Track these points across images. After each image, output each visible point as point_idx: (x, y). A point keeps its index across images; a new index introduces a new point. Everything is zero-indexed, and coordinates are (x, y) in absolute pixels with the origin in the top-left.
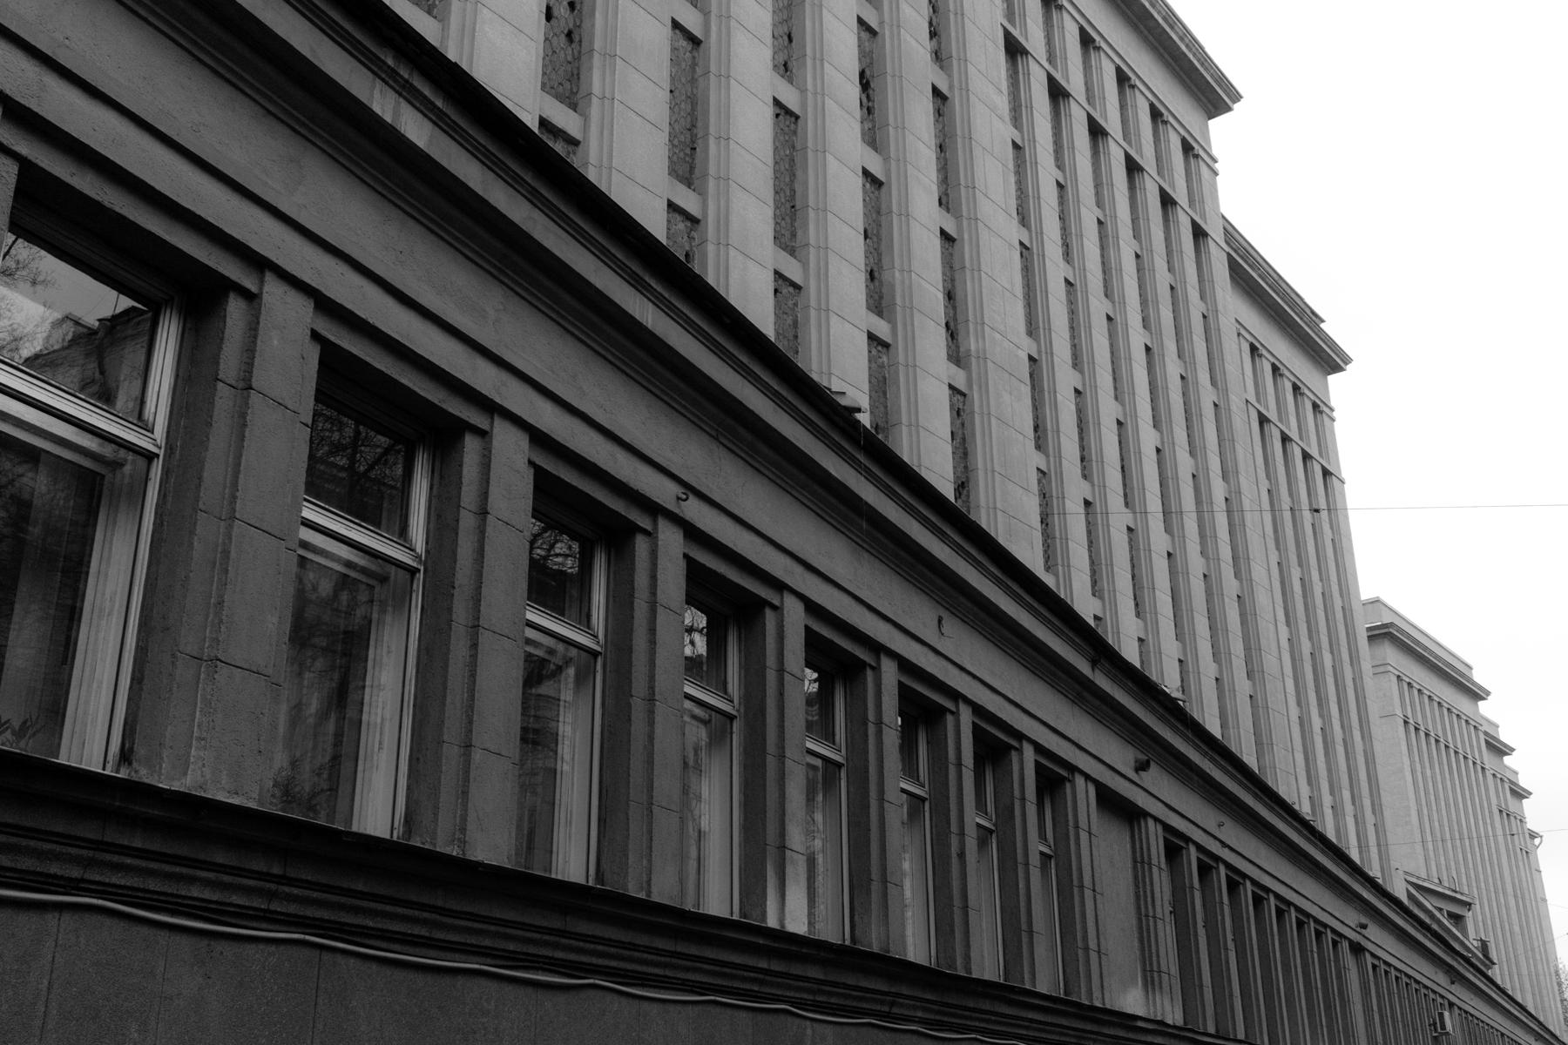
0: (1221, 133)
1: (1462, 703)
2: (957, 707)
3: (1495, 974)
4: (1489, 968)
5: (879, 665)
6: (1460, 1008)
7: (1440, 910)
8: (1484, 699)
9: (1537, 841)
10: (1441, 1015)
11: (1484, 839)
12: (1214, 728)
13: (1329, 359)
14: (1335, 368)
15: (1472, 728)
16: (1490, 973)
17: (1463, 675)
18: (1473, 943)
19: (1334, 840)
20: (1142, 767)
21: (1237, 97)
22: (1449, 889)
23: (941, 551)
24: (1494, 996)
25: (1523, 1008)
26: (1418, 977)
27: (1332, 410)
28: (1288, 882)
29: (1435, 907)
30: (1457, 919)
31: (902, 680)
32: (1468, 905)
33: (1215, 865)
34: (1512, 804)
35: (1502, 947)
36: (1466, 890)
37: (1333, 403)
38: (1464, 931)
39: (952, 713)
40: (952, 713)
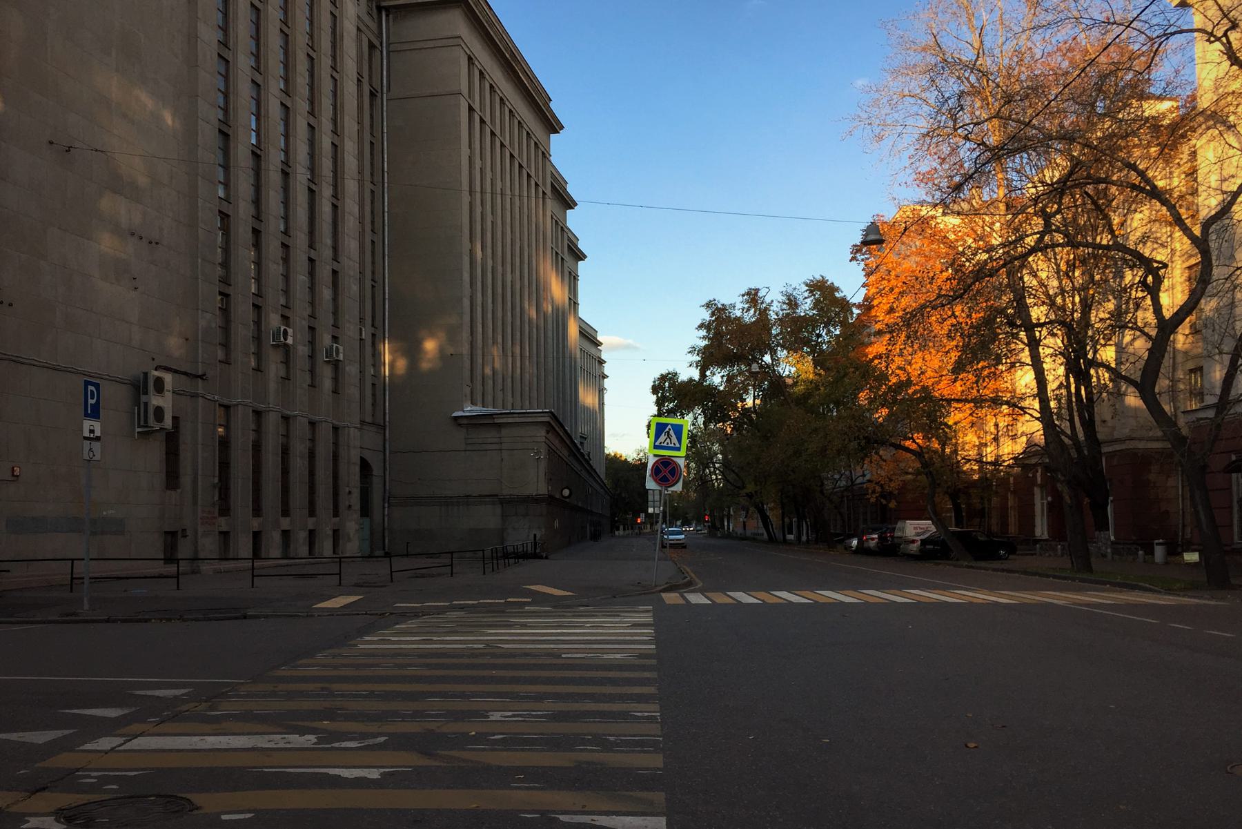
13: (552, 125)
21: (562, 127)
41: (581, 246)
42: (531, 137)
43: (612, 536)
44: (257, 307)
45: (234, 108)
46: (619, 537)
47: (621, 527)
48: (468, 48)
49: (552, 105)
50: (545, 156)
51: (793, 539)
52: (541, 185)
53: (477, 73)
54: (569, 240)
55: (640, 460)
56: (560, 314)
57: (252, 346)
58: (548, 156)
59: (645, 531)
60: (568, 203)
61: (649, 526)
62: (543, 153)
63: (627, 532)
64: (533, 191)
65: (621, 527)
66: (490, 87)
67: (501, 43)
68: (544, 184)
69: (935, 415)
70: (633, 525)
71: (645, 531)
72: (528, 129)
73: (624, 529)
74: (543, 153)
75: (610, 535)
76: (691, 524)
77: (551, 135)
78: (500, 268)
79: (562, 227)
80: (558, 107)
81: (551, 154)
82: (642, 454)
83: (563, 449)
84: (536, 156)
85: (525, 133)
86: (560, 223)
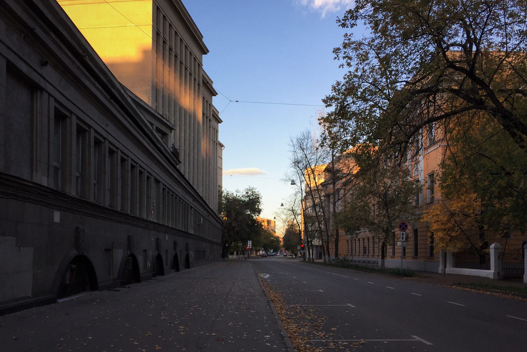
0: (205, 58)
1: (196, 51)
2: (118, 151)
3: (181, 168)
4: (178, 164)
5: (105, 142)
6: (194, 209)
7: (152, 124)
8: (220, 123)
9: (223, 148)
10: (200, 219)
11: (215, 175)
12: (192, 184)
13: (204, 51)
14: (205, 53)
15: (208, 104)
16: (178, 167)
17: (199, 38)
18: (170, 149)
19: (188, 179)
20: (44, 64)
21: (208, 51)
22: (161, 116)
23: (204, 206)
24: (188, 189)
25: (183, 176)
26: (186, 201)
27: (202, 65)
28: (74, 101)
29: (148, 121)
30: (164, 135)
31: (132, 163)
32: (171, 129)
33: (150, 177)
34: (213, 122)
35: (192, 164)
36: (173, 122)
37: (203, 64)
38: (166, 143)
39: (69, 118)
40: (69, 118)
42: (178, 35)
45: (75, 63)
47: (235, 253)
48: (164, 12)
49: (203, 40)
50: (200, 65)
51: (491, 277)
52: (184, 63)
53: (168, 25)
54: (213, 111)
58: (201, 66)
59: (252, 255)
60: (213, 93)
61: (254, 252)
65: (235, 253)
66: (169, 26)
67: (185, 17)
70: (244, 251)
71: (252, 255)
73: (237, 254)
74: (199, 64)
76: (278, 252)
78: (192, 134)
79: (210, 104)
80: (206, 41)
81: (203, 64)
83: (205, 211)
86: (209, 102)
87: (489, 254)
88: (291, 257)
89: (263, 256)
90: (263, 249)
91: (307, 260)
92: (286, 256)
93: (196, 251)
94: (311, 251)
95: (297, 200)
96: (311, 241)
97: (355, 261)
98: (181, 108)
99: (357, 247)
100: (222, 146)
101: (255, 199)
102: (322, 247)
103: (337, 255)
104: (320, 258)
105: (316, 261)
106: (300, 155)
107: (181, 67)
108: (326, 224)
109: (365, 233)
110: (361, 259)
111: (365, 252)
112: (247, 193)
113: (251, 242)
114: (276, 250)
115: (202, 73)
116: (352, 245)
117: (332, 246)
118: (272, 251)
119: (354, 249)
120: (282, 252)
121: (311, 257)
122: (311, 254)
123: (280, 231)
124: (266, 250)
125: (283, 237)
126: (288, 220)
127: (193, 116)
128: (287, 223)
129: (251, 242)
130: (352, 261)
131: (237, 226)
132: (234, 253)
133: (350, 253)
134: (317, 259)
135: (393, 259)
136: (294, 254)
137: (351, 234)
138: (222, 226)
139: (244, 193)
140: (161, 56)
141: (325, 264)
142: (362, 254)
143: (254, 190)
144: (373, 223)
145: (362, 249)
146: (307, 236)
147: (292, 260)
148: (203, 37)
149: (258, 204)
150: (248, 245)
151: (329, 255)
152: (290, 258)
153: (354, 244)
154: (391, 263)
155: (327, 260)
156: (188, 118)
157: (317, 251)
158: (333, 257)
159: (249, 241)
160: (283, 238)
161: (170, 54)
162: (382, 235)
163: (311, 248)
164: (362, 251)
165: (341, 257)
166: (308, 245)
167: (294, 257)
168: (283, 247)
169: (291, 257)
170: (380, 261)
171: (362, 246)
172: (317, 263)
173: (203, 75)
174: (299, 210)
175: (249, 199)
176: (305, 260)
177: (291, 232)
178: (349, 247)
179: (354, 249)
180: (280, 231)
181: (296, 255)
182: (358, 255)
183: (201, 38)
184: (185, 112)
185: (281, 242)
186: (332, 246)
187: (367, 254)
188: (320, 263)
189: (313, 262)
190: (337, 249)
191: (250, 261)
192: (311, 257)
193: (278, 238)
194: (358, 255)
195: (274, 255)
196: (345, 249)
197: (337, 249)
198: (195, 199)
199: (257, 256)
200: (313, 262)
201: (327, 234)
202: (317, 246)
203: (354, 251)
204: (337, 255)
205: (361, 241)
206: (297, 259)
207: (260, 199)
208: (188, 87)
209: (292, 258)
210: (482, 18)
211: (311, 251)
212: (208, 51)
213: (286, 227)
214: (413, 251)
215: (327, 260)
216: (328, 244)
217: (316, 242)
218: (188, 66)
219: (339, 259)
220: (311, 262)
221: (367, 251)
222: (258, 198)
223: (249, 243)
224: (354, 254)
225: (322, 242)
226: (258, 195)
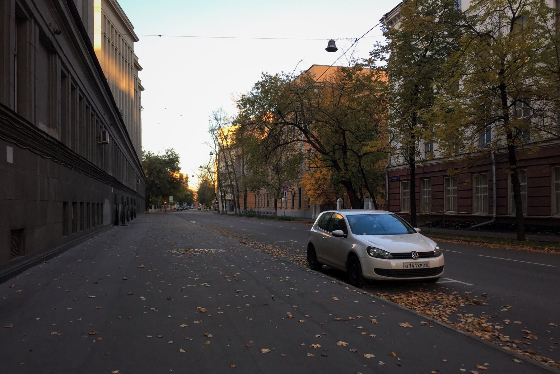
1: (128, 39)
9: (142, 109)
13: (135, 39)
37: (134, 50)
41: (140, 62)
43: (147, 213)
44: (310, 222)
46: (150, 213)
47: (153, 206)
49: (135, 30)
50: (132, 51)
53: (111, 26)
55: (169, 156)
56: (115, 87)
57: (431, 244)
62: (131, 51)
63: (157, 210)
64: (128, 67)
65: (153, 206)
68: (132, 63)
69: (542, 57)
72: (108, 19)
73: (155, 208)
74: (131, 51)
75: (145, 212)
77: (134, 43)
80: (137, 31)
82: (170, 153)
84: (119, 41)
85: (111, 26)
87: (336, 205)
88: (206, 210)
89: (178, 210)
90: (178, 203)
91: (221, 212)
92: (200, 209)
93: (65, 203)
94: (224, 204)
95: (212, 161)
96: (225, 196)
97: (261, 213)
98: (120, 91)
99: (263, 200)
100: (142, 107)
101: (175, 158)
102: (234, 200)
103: (245, 207)
104: (233, 211)
105: (228, 213)
106: (215, 124)
107: (116, 53)
108: (236, 181)
109: (263, 191)
110: (265, 210)
111: (268, 205)
112: (167, 153)
113: (172, 197)
114: (189, 204)
115: (133, 56)
116: (258, 200)
117: (241, 201)
118: (185, 205)
119: (260, 202)
120: (195, 206)
121: (225, 210)
122: (224, 207)
123: (194, 185)
124: (181, 204)
125: (198, 191)
126: (202, 176)
127: (128, 95)
128: (202, 179)
129: (172, 197)
130: (258, 212)
131: (159, 183)
132: (153, 207)
133: (257, 206)
134: (230, 211)
135: (293, 210)
136: (208, 207)
137: (254, 192)
138: (146, 182)
139: (165, 154)
140: (107, 53)
141: (236, 215)
142: (266, 206)
143: (173, 151)
144: (269, 185)
145: (266, 202)
146: (221, 191)
147: (208, 213)
148: (133, 28)
149: (177, 163)
150: (170, 200)
151: (239, 208)
152: (204, 211)
153: (260, 199)
154: (280, 213)
155: (238, 212)
156: (125, 97)
157: (230, 205)
158: (242, 209)
159: (170, 196)
160: (198, 193)
161: (112, 49)
162: (275, 191)
163: (224, 201)
164: (266, 204)
165: (248, 209)
166: (222, 199)
167: (208, 210)
168: (198, 200)
169: (206, 210)
170: (274, 211)
171: (266, 200)
172: (229, 215)
173: (134, 59)
174: (214, 169)
175: (169, 158)
176: (219, 212)
177: (205, 186)
178: (256, 201)
179: (260, 202)
180: (194, 185)
181: (210, 208)
182: (264, 208)
183: (132, 28)
184: (123, 93)
185: (194, 196)
186: (241, 201)
187: (270, 206)
188: (232, 215)
189: (227, 214)
190: (245, 203)
191: (173, 214)
192: (225, 210)
193: (191, 192)
194: (264, 208)
195: (188, 209)
196: (253, 201)
197: (245, 203)
198: (137, 166)
199: (172, 209)
200: (227, 214)
201: (238, 190)
202: (230, 200)
203: (260, 204)
204: (245, 207)
205: (263, 197)
206: (212, 211)
207: (179, 158)
208: (124, 73)
209: (207, 211)
210: (277, 130)
211: (224, 204)
212: (138, 40)
213: (201, 182)
214: (298, 203)
215: (238, 212)
216: (238, 199)
217: (229, 196)
218: (130, 62)
219: (247, 210)
220: (224, 213)
221: (270, 204)
222: (177, 157)
223: (170, 198)
224: (260, 206)
225: (234, 197)
226: (177, 155)
